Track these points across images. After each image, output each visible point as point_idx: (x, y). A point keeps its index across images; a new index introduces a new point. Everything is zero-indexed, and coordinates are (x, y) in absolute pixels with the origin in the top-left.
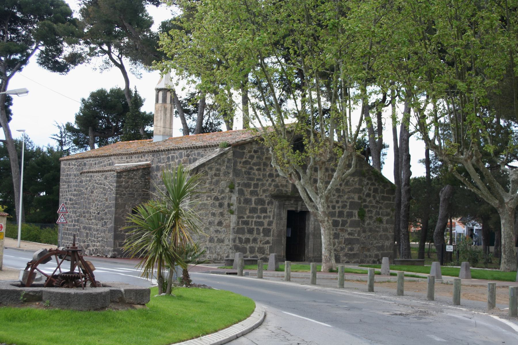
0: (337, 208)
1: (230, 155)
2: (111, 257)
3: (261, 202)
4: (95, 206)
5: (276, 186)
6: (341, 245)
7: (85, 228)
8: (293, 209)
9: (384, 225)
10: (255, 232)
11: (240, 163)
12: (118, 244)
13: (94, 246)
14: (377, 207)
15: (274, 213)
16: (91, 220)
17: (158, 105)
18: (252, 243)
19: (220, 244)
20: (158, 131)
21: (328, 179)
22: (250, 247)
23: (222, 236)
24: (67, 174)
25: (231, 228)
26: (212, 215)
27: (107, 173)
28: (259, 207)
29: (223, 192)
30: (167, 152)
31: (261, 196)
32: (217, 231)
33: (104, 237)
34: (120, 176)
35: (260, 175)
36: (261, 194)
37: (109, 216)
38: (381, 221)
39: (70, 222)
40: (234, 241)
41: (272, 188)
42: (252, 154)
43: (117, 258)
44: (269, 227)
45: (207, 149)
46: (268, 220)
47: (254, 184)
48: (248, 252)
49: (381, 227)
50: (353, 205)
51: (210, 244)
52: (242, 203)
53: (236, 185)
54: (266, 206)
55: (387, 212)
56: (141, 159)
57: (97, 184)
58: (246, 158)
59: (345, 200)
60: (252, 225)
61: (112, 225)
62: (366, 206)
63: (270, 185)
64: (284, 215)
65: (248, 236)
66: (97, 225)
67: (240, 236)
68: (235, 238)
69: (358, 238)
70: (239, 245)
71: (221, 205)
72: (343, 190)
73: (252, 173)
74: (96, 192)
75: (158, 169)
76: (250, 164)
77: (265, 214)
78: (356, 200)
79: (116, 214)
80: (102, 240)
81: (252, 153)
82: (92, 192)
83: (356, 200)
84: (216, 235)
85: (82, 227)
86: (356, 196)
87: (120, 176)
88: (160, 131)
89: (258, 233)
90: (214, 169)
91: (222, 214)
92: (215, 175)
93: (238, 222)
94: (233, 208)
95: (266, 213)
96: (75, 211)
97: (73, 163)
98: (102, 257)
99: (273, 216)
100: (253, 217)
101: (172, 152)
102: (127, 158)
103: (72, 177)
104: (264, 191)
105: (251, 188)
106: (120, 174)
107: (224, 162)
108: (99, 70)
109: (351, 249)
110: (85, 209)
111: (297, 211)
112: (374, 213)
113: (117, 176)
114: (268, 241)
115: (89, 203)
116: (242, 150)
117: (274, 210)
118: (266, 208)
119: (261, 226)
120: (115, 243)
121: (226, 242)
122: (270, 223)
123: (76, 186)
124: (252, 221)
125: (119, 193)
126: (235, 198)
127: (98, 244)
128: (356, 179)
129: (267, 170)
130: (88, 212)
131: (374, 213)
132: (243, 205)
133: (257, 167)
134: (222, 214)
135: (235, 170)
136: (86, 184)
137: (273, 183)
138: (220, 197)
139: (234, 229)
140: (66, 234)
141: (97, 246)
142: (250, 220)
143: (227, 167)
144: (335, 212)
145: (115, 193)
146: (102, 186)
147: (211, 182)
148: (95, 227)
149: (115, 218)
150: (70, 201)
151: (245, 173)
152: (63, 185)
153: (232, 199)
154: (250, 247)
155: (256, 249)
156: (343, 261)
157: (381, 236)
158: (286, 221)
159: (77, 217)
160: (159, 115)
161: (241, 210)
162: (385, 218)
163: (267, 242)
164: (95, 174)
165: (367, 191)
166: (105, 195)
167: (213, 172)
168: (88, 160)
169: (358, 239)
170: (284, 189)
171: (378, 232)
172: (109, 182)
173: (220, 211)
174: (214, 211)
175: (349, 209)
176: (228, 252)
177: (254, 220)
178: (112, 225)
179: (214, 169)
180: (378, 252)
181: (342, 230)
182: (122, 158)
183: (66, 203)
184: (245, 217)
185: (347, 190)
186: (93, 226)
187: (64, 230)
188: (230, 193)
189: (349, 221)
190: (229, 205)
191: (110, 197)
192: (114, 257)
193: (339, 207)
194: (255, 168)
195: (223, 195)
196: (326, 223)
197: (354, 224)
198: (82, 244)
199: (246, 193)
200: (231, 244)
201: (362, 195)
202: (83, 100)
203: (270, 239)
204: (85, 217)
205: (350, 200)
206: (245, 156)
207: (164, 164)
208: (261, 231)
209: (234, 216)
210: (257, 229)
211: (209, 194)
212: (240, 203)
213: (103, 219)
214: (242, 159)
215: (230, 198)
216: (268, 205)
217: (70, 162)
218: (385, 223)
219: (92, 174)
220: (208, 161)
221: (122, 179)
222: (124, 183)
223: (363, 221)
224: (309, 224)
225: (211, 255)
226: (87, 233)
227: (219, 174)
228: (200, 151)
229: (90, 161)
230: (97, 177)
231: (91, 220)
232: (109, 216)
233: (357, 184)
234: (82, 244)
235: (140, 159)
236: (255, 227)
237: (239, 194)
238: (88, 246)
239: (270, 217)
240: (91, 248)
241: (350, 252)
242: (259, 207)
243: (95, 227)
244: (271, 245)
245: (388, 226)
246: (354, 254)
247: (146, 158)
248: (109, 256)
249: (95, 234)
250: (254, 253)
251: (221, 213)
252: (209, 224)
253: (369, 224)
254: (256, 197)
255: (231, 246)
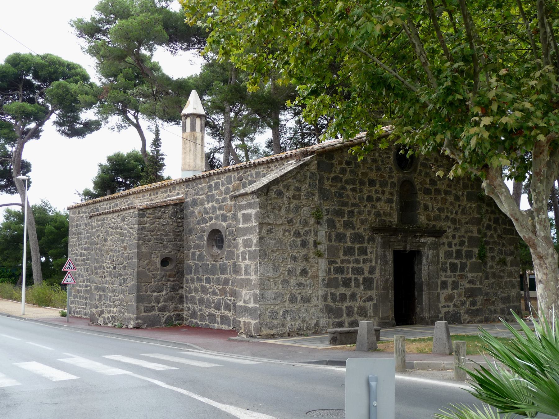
0: (453, 246)
1: (313, 167)
2: (134, 328)
3: (358, 238)
4: (110, 259)
5: (378, 215)
6: (460, 299)
7: (97, 288)
8: (401, 248)
9: (509, 268)
10: (353, 284)
11: (328, 179)
12: (142, 308)
13: (109, 312)
14: (499, 244)
15: (377, 254)
16: (105, 277)
17: (185, 135)
18: (350, 301)
19: (306, 305)
20: (187, 166)
21: (442, 204)
22: (347, 307)
23: (308, 292)
24: (77, 224)
25: (320, 278)
26: (292, 260)
27: (125, 212)
28: (357, 246)
29: (306, 223)
30: (207, 179)
31: (358, 229)
32: (300, 285)
33: (122, 300)
34: (143, 214)
35: (355, 198)
36: (358, 227)
37: (129, 271)
38: (503, 262)
39: (81, 282)
40: (325, 300)
41: (372, 217)
42: (343, 166)
43: (142, 328)
44: (370, 276)
45: (272, 166)
46: (368, 265)
47: (349, 212)
48: (345, 315)
49: (506, 272)
50: (472, 241)
51: (291, 305)
52: (333, 241)
53: (324, 213)
54: (366, 244)
55: (510, 250)
56: (170, 194)
57: (112, 228)
58: (335, 172)
59: (463, 234)
60: (348, 273)
61: (133, 282)
62: (487, 243)
63: (369, 213)
64: (390, 257)
65: (343, 290)
66: (112, 283)
67: (333, 291)
68: (326, 295)
69: (481, 286)
70: (332, 304)
71: (304, 244)
72: (459, 220)
73: (344, 195)
74: (111, 240)
75: (195, 203)
76: (341, 181)
77: (365, 257)
78: (475, 234)
79: (139, 266)
80: (120, 305)
81: (344, 166)
82: (106, 240)
83: (475, 234)
84: (299, 291)
85: (93, 287)
86: (475, 229)
87: (143, 214)
88: (189, 165)
89: (357, 286)
90: (292, 188)
91: (306, 258)
92: (294, 197)
93: (329, 269)
94: (321, 248)
95: (367, 255)
96: (87, 269)
97: (84, 210)
98: (121, 327)
99: (376, 258)
100: (349, 262)
101: (215, 177)
102: (150, 195)
103: (82, 227)
104: (362, 222)
105: (344, 217)
106: (143, 212)
107: (306, 177)
108: (116, 129)
109: (473, 303)
110: (97, 263)
111: (406, 251)
112: (496, 252)
113: (139, 214)
114: (371, 296)
115: (102, 255)
116: (329, 160)
117: (376, 250)
118: (366, 247)
119: (360, 274)
120: (138, 308)
121: (314, 301)
122: (372, 270)
123: (88, 238)
124: (348, 268)
125: (142, 239)
126: (324, 233)
127: (115, 309)
128: (474, 206)
129: (365, 190)
130: (100, 267)
131: (496, 252)
132: (335, 244)
133: (352, 186)
134: (306, 258)
135: (321, 190)
136: (97, 231)
137: (374, 211)
138: (302, 232)
139: (324, 280)
140: (77, 297)
141: (113, 313)
142: (345, 265)
143: (310, 185)
144: (452, 251)
145: (137, 239)
146: (119, 230)
147: (289, 207)
148: (110, 286)
149: (138, 273)
150: (81, 256)
151: (335, 195)
152: (72, 238)
153: (319, 234)
154: (347, 307)
155: (356, 309)
156: (465, 320)
157: (505, 282)
158: (393, 265)
159: (89, 275)
160: (188, 146)
161: (332, 251)
162: (509, 259)
163: (370, 299)
164: (109, 216)
165: (487, 222)
166: (123, 242)
167: (291, 193)
168: (101, 204)
169: (480, 289)
170: (388, 219)
171: (502, 277)
172: (127, 225)
173: (303, 253)
174: (294, 254)
175: (469, 247)
176: (318, 316)
177: (351, 265)
178: (134, 282)
179: (292, 188)
180: (504, 306)
181: (461, 277)
182: (143, 196)
183: (76, 260)
184: (339, 261)
185: (464, 221)
186: (107, 286)
187: (75, 292)
188: (316, 226)
189: (468, 264)
190: (316, 244)
191: (130, 245)
192: (137, 327)
193: (455, 245)
194: (349, 187)
195: (306, 229)
196: (550, 259)
197: (475, 268)
198: (94, 310)
199: (338, 225)
200: (321, 304)
201: (481, 227)
202: (100, 165)
203: (373, 293)
204: (96, 274)
205: (469, 234)
206: (333, 169)
207: (203, 196)
208: (361, 282)
209: (324, 260)
210: (356, 279)
211: (287, 227)
212: (330, 241)
213: (120, 275)
214: (330, 173)
215: (317, 233)
216: (368, 243)
217: (79, 209)
218: (509, 265)
219: (105, 216)
220: (283, 176)
221: (145, 219)
222: (148, 225)
223: (485, 264)
224: (421, 269)
225: (293, 323)
226: (100, 296)
227: (299, 195)
228: (260, 169)
229: (104, 204)
230: (111, 219)
231: (105, 277)
232: (129, 271)
233: (475, 211)
234: (94, 310)
235: (169, 193)
236: (353, 277)
237: (328, 226)
238: (102, 312)
239: (371, 261)
240: (106, 315)
241: (472, 308)
242: (357, 246)
243: (110, 286)
244: (375, 302)
245: (512, 268)
246: (477, 310)
247: (177, 191)
248: (130, 326)
249: (110, 296)
250: (352, 316)
251: (305, 255)
252: (289, 274)
253: (491, 267)
254: (352, 232)
255: (321, 307)
